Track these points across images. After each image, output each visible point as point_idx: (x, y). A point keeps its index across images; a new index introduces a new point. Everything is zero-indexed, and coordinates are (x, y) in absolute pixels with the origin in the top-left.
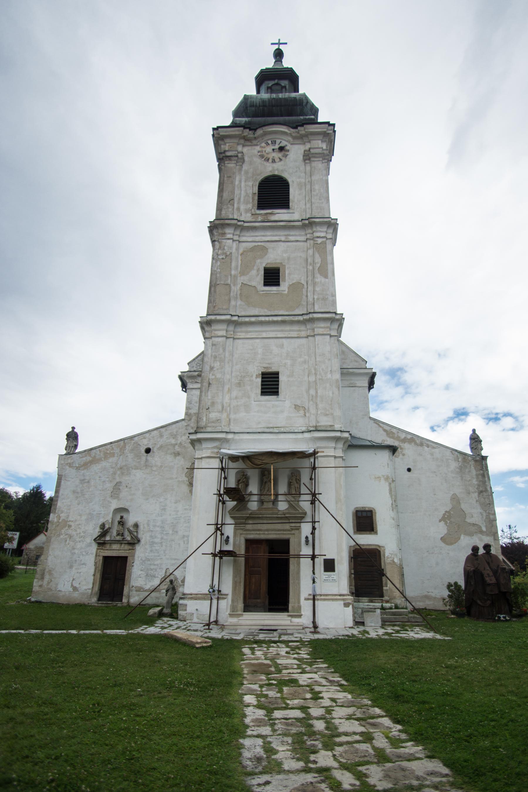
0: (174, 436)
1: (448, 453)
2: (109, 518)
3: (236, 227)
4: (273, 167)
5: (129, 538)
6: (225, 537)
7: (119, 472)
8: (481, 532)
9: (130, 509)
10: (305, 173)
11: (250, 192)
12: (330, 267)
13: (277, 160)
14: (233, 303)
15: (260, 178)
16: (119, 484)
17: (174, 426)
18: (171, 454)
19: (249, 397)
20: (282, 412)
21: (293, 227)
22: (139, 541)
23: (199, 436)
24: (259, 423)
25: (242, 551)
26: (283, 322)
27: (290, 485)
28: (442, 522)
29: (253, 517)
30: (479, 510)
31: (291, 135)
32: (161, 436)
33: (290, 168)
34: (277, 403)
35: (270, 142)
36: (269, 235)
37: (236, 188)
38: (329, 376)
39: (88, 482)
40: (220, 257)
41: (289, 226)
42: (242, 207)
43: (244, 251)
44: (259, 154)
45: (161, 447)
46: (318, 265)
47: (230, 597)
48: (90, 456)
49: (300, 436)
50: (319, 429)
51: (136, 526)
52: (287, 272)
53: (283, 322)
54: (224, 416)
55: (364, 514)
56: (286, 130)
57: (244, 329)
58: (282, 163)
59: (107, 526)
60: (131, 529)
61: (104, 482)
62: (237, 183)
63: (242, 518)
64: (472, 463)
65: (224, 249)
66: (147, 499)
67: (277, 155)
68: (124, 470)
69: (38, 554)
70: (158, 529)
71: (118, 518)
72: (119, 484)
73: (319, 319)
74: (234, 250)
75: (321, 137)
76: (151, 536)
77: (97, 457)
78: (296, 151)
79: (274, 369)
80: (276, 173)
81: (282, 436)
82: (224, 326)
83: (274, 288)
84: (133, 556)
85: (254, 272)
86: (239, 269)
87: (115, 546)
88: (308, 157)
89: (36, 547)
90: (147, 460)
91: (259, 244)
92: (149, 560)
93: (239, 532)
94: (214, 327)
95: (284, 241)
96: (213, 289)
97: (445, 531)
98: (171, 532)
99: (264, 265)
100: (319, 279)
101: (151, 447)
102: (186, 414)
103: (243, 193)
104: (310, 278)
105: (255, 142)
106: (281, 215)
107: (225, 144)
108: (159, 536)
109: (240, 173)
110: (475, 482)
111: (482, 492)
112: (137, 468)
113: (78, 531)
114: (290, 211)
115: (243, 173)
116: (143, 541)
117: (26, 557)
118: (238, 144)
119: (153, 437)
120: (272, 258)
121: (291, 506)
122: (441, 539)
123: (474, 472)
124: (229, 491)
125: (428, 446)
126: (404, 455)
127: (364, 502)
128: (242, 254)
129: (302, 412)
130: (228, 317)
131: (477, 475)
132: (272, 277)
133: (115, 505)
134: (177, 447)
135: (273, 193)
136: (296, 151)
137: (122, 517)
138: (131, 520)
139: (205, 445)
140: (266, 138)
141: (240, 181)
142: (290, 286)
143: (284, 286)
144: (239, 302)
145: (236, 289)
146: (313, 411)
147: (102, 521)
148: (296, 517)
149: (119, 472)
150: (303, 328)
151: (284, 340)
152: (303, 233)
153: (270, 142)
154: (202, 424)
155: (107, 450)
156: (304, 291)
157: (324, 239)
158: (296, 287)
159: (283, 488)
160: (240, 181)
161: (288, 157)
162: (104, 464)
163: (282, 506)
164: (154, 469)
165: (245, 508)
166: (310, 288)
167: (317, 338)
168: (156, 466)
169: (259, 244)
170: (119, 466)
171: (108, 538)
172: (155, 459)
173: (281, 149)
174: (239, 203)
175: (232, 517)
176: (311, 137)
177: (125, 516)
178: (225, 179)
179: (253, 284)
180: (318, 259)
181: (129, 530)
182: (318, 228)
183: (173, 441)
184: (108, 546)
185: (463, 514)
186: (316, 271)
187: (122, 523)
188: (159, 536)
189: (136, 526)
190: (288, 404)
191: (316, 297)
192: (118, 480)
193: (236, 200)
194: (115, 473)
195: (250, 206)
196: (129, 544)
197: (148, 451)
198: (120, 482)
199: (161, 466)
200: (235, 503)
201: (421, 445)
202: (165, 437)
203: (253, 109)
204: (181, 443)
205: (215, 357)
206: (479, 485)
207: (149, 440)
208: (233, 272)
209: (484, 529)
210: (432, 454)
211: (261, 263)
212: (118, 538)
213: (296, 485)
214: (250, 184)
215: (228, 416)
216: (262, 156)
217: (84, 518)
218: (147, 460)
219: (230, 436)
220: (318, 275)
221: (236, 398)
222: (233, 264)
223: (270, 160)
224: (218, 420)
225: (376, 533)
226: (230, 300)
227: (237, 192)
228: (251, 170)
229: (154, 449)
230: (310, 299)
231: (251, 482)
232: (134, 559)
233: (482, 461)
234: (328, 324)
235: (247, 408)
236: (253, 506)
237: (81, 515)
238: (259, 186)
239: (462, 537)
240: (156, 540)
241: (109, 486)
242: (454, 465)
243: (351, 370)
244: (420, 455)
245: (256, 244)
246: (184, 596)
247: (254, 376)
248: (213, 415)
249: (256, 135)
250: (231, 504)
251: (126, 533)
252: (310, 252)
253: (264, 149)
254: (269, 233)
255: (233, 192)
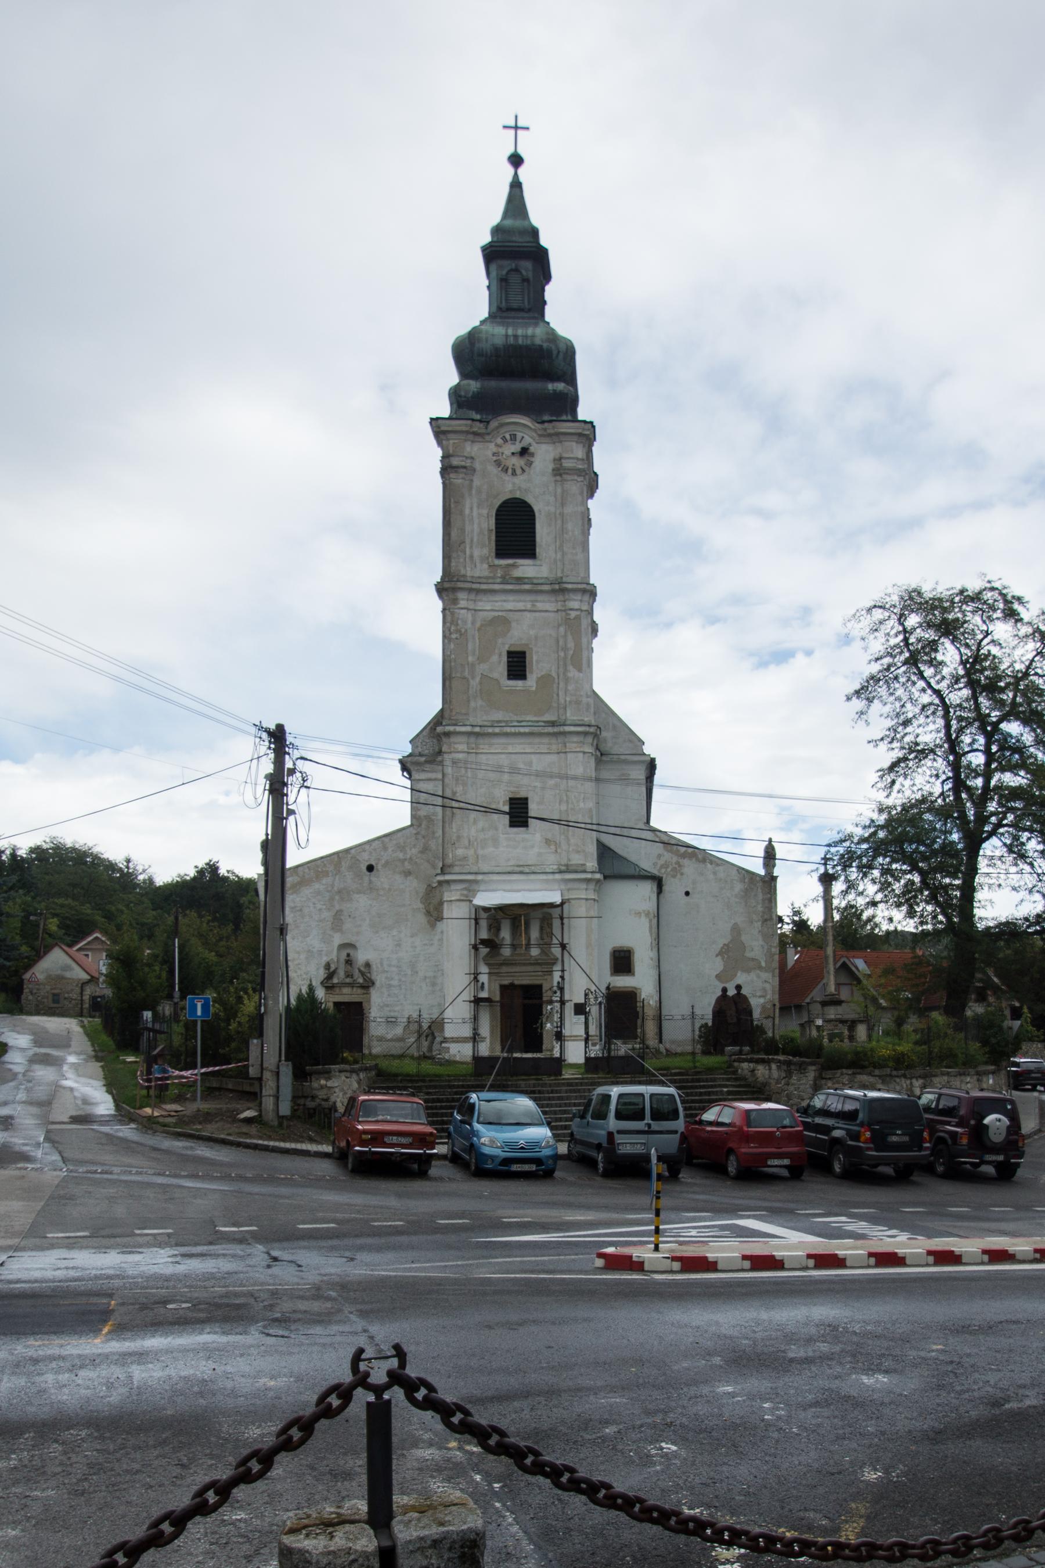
0: (402, 848)
1: (734, 872)
2: (334, 956)
3: (470, 590)
4: (514, 484)
5: (361, 980)
6: (480, 984)
7: (337, 897)
8: (760, 968)
9: (357, 945)
10: (555, 496)
11: (485, 526)
12: (585, 654)
13: (518, 471)
14: (473, 704)
15: (497, 503)
16: (339, 912)
17: (400, 834)
18: (400, 873)
19: (497, 829)
20: (532, 847)
21: (541, 592)
22: (373, 983)
23: (448, 877)
24: (509, 860)
25: (497, 998)
26: (531, 734)
27: (542, 929)
28: (719, 957)
29: (507, 963)
30: (761, 942)
31: (535, 431)
32: (385, 848)
33: (535, 486)
34: (526, 836)
35: (508, 437)
36: (511, 603)
37: (467, 522)
38: (582, 805)
39: (301, 910)
40: (454, 636)
41: (533, 588)
42: (477, 553)
43: (482, 625)
44: (495, 458)
45: (387, 863)
46: (571, 652)
47: (488, 1040)
48: (297, 875)
49: (551, 877)
50: (571, 868)
51: (368, 965)
52: (535, 658)
53: (531, 734)
54: (471, 852)
55: (622, 954)
56: (530, 424)
57: (487, 740)
58: (524, 477)
59: (333, 967)
60: (362, 969)
61: (320, 910)
62: (467, 511)
63: (497, 964)
64: (760, 884)
65: (457, 625)
66: (377, 932)
67: (517, 462)
68: (344, 894)
69: (56, 991)
70: (394, 969)
71: (343, 956)
72: (339, 912)
73: (570, 733)
74: (469, 625)
75: (575, 438)
76: (386, 978)
77: (307, 877)
78: (544, 454)
79: (522, 795)
80: (518, 495)
81: (533, 877)
82: (464, 739)
83: (519, 683)
84: (369, 1001)
85: (495, 658)
86: (477, 652)
87: (346, 990)
88: (559, 471)
89: (49, 977)
90: (370, 882)
91: (500, 614)
92: (387, 1006)
93: (494, 977)
94: (453, 739)
95: (530, 611)
96: (447, 683)
97: (722, 968)
98: (409, 972)
99: (507, 648)
100: (572, 673)
101: (373, 863)
102: (413, 817)
103: (476, 526)
104: (561, 670)
105: (487, 438)
106: (525, 568)
107: (448, 440)
108: (397, 978)
109: (470, 495)
110: (760, 908)
111: (766, 920)
112: (359, 892)
113: (299, 972)
114: (538, 562)
115: (474, 492)
116: (378, 984)
117: (30, 997)
118: (466, 440)
119: (375, 850)
120: (517, 636)
121: (543, 952)
122: (717, 976)
123: (760, 896)
124: (484, 942)
125: (711, 863)
126: (682, 874)
127: (623, 941)
128: (479, 630)
129: (553, 847)
130: (468, 729)
131: (763, 900)
132: (517, 665)
133: (338, 940)
134: (406, 863)
135: (516, 530)
136: (544, 454)
137: (348, 955)
138: (361, 957)
139: (453, 887)
140: (502, 430)
141: (471, 509)
142: (539, 680)
143: (531, 682)
144: (480, 703)
145: (475, 683)
146: (564, 847)
147: (325, 959)
148: (547, 963)
149: (337, 897)
150: (554, 740)
151: (533, 756)
152: (553, 599)
153: (508, 437)
154: (449, 861)
155: (318, 866)
156: (555, 686)
157: (578, 613)
158: (545, 681)
159: (535, 934)
160: (471, 509)
161: (534, 465)
162: (317, 886)
163: (535, 952)
164: (382, 893)
165: (499, 954)
166: (562, 685)
167: (569, 755)
168: (384, 889)
169: (500, 614)
170: (336, 888)
171: (335, 981)
172: (382, 879)
173: (524, 452)
174: (471, 547)
175: (488, 964)
176: (562, 438)
177: (352, 952)
178: (452, 506)
179: (495, 675)
180: (571, 644)
181: (360, 971)
182: (572, 596)
183: (401, 855)
184: (337, 990)
185: (742, 947)
186: (569, 662)
187: (349, 962)
188: (397, 978)
189: (368, 965)
190: (538, 837)
191: (568, 699)
192: (337, 907)
193: (468, 541)
194: (332, 899)
195: (485, 551)
196: (363, 987)
197: (370, 868)
198: (341, 911)
199: (390, 890)
200: (488, 949)
201: (704, 861)
202: (390, 850)
203: (483, 359)
204: (411, 858)
205: (457, 780)
206: (764, 912)
207: (371, 853)
208: (470, 659)
209: (763, 964)
210: (715, 873)
211: (503, 644)
212: (348, 980)
213: (549, 930)
214: (485, 512)
215: (475, 851)
216: (498, 463)
217: (303, 956)
218: (370, 882)
219: (480, 877)
220: (570, 668)
221: (483, 830)
222: (470, 646)
223: (510, 471)
224: (465, 858)
225: (633, 975)
226: (469, 701)
227: (468, 528)
228: (485, 487)
229: (379, 867)
230: (562, 701)
231: (503, 926)
232: (369, 1004)
233: (770, 881)
234: (581, 738)
235: (495, 842)
236: (506, 952)
237: (298, 953)
238: (497, 515)
239: (739, 974)
240: (392, 982)
241: (327, 915)
242: (739, 887)
243: (623, 757)
244: (702, 874)
245: (496, 614)
246: (445, 1040)
247: (501, 803)
248: (460, 852)
249: (489, 430)
250: (484, 951)
251: (356, 974)
252: (562, 629)
253: (500, 450)
254: (511, 598)
255: (462, 530)
